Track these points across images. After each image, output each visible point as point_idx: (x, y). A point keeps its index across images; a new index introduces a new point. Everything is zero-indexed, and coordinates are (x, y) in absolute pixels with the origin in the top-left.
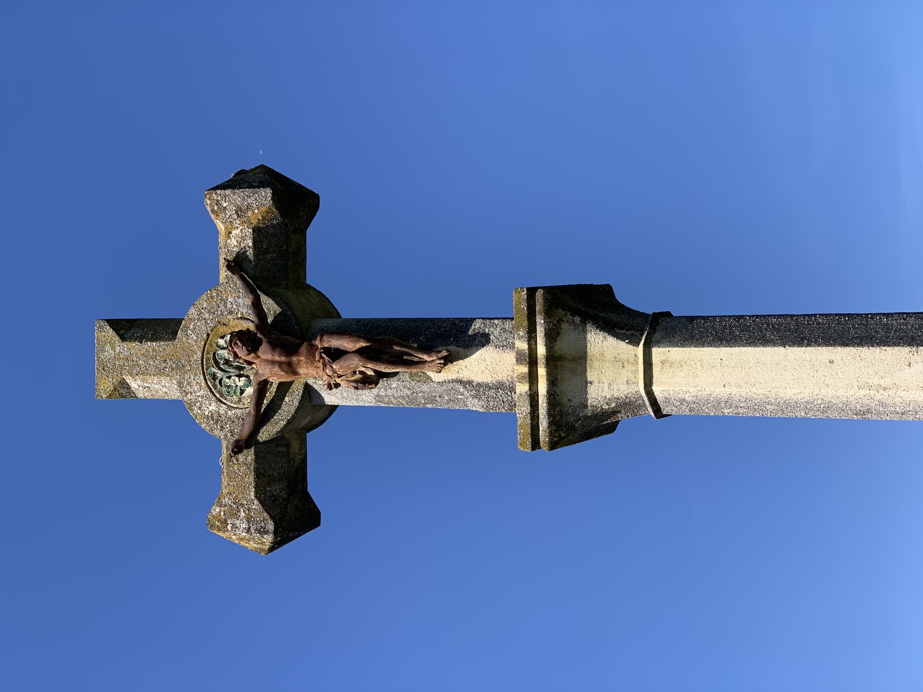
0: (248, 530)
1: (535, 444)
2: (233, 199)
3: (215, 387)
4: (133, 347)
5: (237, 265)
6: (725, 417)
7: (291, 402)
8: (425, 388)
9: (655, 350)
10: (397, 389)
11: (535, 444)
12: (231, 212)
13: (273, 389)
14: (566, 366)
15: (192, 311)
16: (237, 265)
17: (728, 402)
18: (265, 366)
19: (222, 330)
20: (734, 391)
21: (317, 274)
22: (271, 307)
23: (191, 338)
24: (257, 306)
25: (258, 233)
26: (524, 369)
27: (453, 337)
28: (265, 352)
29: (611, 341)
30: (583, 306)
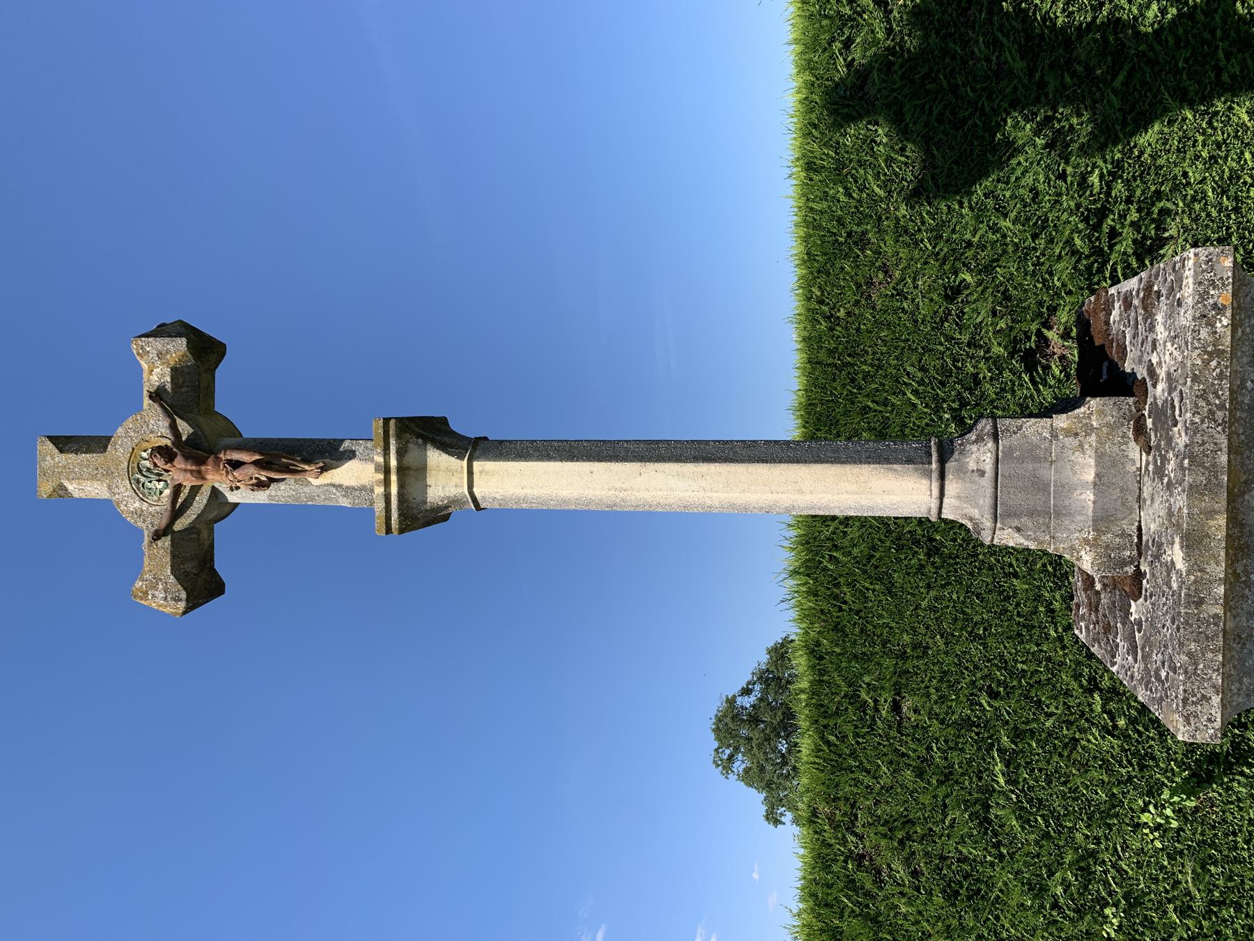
0: (165, 599)
1: (389, 530)
7: (201, 501)
8: (306, 490)
10: (285, 491)
12: (153, 354)
13: (186, 491)
14: (412, 474)
15: (120, 430)
17: (525, 500)
18: (180, 473)
19: (145, 445)
20: (529, 492)
22: (185, 428)
23: (119, 451)
24: (173, 427)
25: (175, 371)
26: (381, 476)
27: (328, 453)
28: (179, 462)
29: (445, 456)
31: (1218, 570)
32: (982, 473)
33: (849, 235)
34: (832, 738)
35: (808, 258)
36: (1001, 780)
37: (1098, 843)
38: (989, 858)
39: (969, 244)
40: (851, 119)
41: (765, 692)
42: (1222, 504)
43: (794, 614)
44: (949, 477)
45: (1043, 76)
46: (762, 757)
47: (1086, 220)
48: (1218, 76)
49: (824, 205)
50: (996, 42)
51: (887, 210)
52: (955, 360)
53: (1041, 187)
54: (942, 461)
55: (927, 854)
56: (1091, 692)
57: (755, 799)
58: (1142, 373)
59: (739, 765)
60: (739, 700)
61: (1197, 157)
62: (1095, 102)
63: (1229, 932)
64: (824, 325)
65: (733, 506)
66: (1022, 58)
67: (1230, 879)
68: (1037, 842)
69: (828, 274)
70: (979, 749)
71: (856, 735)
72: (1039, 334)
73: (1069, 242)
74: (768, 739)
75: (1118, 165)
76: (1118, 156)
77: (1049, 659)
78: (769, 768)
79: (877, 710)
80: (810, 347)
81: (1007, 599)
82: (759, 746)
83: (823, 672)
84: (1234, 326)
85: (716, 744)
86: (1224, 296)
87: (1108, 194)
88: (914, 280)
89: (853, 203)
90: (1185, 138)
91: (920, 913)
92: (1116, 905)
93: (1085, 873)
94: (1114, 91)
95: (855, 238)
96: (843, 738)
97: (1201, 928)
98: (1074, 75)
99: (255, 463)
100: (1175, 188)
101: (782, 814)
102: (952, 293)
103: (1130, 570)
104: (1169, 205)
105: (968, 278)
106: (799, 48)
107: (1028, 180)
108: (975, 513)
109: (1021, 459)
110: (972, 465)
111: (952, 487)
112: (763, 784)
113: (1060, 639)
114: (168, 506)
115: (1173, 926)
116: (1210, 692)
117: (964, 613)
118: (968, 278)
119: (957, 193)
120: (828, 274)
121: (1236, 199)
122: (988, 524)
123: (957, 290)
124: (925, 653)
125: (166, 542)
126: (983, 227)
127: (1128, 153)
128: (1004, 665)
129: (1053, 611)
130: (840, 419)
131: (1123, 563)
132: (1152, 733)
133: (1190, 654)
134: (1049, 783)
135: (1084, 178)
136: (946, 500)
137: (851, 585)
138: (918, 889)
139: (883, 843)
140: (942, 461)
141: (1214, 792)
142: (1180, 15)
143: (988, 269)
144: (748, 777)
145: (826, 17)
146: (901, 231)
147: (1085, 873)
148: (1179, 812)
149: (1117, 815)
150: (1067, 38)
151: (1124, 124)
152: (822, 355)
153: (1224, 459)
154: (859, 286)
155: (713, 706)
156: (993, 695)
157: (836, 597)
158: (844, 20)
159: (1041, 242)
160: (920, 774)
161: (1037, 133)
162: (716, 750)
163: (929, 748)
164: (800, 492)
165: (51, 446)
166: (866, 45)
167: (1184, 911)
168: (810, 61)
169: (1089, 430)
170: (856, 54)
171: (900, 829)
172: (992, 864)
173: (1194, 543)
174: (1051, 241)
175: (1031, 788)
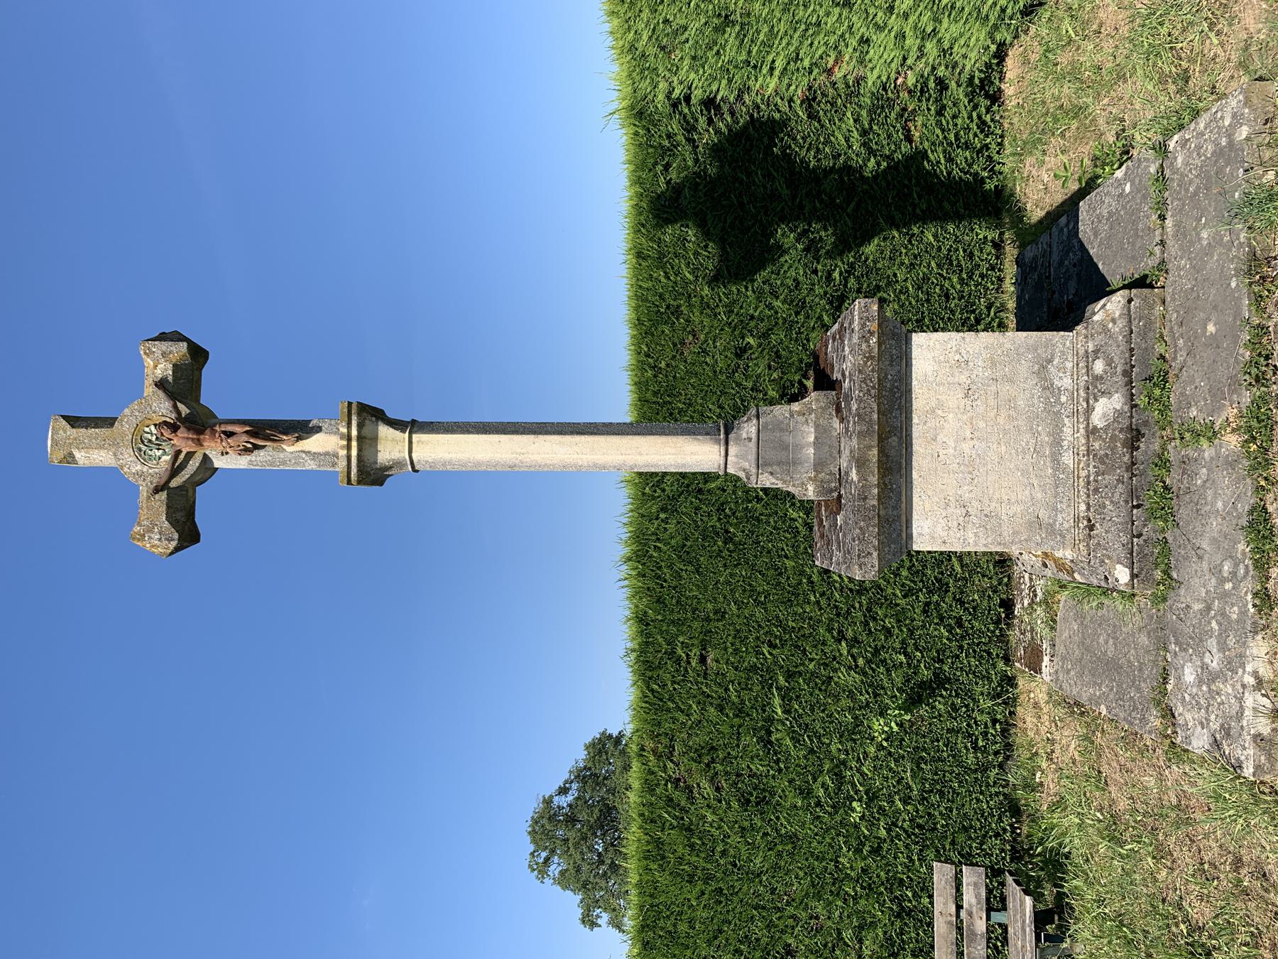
1: (349, 482)
3: (141, 455)
4: (72, 432)
5: (161, 384)
7: (194, 464)
8: (281, 455)
9: (414, 436)
10: (265, 458)
11: (349, 482)
12: (158, 354)
13: (182, 456)
14: (367, 442)
15: (127, 411)
16: (161, 384)
18: (182, 441)
19: (148, 422)
20: (453, 456)
21: (208, 397)
22: (184, 410)
23: (125, 426)
24: (175, 407)
27: (302, 429)
28: (182, 432)
29: (391, 430)
30: (371, 414)
31: (874, 479)
32: (750, 439)
33: (668, 307)
34: (655, 687)
35: (638, 323)
36: (779, 711)
37: (848, 754)
39: (752, 317)
40: (668, 221)
41: (582, 790)
42: (875, 443)
43: (627, 592)
44: (731, 443)
45: (801, 201)
46: (578, 857)
47: (831, 303)
48: (914, 210)
49: (650, 284)
50: (770, 174)
52: (743, 401)
53: (801, 279)
54: (727, 434)
55: (727, 773)
57: (571, 901)
58: (840, 377)
59: (554, 869)
60: (556, 799)
62: (836, 222)
64: (650, 373)
65: (595, 465)
67: (936, 774)
68: (805, 757)
69: (653, 335)
70: (763, 688)
71: (674, 682)
72: (800, 382)
73: (820, 318)
74: (585, 838)
75: (852, 266)
76: (851, 260)
78: (585, 868)
79: (689, 663)
80: (640, 389)
81: (780, 574)
82: (577, 845)
83: (648, 635)
84: (880, 344)
85: (532, 848)
86: (873, 326)
87: (845, 286)
89: (671, 284)
90: (894, 250)
92: (860, 800)
93: (839, 778)
94: (848, 215)
95: (672, 309)
99: (246, 432)
100: (889, 284)
101: (598, 917)
102: (741, 352)
103: (835, 494)
104: (885, 295)
106: (632, 167)
107: (792, 273)
108: (746, 465)
109: (773, 430)
110: (745, 436)
112: (579, 885)
113: (818, 602)
114: (168, 467)
115: (898, 812)
116: (872, 550)
117: (750, 585)
119: (744, 280)
120: (653, 335)
121: (928, 293)
122: (754, 471)
124: (723, 617)
126: (762, 306)
127: (857, 258)
128: (780, 624)
130: (660, 408)
131: (832, 491)
132: (882, 669)
133: (861, 528)
134: (812, 710)
135: (829, 274)
136: (729, 458)
137: (670, 567)
138: (720, 801)
139: (694, 765)
141: (923, 710)
142: (889, 167)
143: (765, 335)
144: (564, 880)
146: (705, 306)
148: (900, 725)
150: (817, 177)
151: (855, 238)
152: (649, 395)
153: (876, 416)
154: (675, 345)
155: (530, 807)
156: (772, 645)
157: (659, 577)
158: (664, 151)
160: (721, 709)
161: (798, 240)
162: (532, 854)
163: (727, 690)
165: (64, 422)
166: (681, 169)
167: (905, 801)
168: (640, 177)
169: (811, 411)
170: (673, 175)
171: (706, 754)
172: (773, 777)
173: (861, 463)
175: (800, 716)
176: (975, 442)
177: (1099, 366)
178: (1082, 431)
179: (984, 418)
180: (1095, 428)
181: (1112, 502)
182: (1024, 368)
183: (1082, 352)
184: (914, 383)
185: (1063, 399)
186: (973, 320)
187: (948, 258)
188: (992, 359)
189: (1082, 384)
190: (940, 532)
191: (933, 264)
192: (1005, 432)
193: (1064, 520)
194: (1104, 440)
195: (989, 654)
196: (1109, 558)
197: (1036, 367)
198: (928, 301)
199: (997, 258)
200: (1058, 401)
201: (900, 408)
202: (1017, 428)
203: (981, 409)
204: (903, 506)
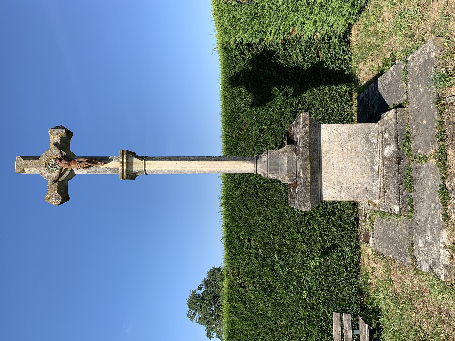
0: (55, 200)
1: (123, 178)
2: (55, 131)
3: (48, 170)
6: (158, 174)
7: (67, 173)
8: (99, 169)
10: (93, 170)
11: (123, 178)
13: (63, 170)
14: (129, 164)
15: (44, 154)
16: (56, 144)
17: (159, 171)
18: (63, 164)
19: (51, 158)
20: (160, 169)
22: (64, 153)
23: (43, 159)
24: (61, 152)
25: (61, 138)
26: (121, 164)
27: (106, 160)
28: (63, 161)
29: (138, 160)
30: (131, 154)
31: (309, 176)
32: (265, 162)
33: (235, 115)
34: (233, 250)
35: (225, 121)
36: (277, 258)
37: (301, 274)
38: (274, 281)
39: (265, 119)
40: (235, 86)
41: (206, 288)
42: (309, 163)
44: (258, 163)
47: (292, 114)
48: (321, 81)
50: (270, 69)
51: (245, 110)
52: (262, 148)
53: (282, 105)
54: (257, 160)
56: (298, 233)
57: (203, 329)
58: (296, 140)
59: (197, 317)
60: (197, 291)
61: (317, 100)
63: (333, 294)
64: (229, 139)
65: (210, 171)
66: (277, 74)
67: (333, 280)
68: (286, 275)
69: (230, 125)
70: (271, 250)
71: (239, 249)
72: (282, 141)
73: (289, 119)
74: (207, 306)
75: (299, 100)
77: (287, 225)
78: (208, 316)
79: (244, 241)
80: (226, 144)
81: (276, 209)
83: (230, 232)
84: (310, 128)
85: (188, 309)
86: (307, 122)
87: (297, 108)
88: (252, 127)
90: (314, 95)
91: (257, 298)
92: (306, 290)
93: (298, 282)
94: (298, 83)
96: (236, 250)
97: (326, 294)
98: (288, 78)
99: (86, 161)
100: (313, 107)
101: (213, 334)
102: (261, 131)
103: (295, 181)
104: (311, 111)
105: (265, 127)
106: (222, 67)
107: (279, 103)
108: (264, 171)
109: (273, 158)
110: (263, 160)
111: (259, 165)
112: (206, 323)
113: (290, 219)
115: (320, 294)
116: (308, 201)
118: (265, 127)
119: (262, 106)
120: (230, 125)
121: (326, 110)
122: (266, 173)
123: (262, 130)
124: (256, 225)
125: (56, 184)
126: (268, 115)
127: (302, 98)
128: (277, 227)
129: (288, 212)
130: (233, 151)
131: (294, 180)
132: (313, 243)
133: (304, 193)
134: (289, 258)
137: (237, 207)
138: (256, 291)
140: (257, 160)
141: (328, 257)
142: (312, 66)
143: (270, 125)
144: (200, 321)
145: (229, 60)
146: (248, 115)
147: (298, 282)
148: (320, 263)
149: (306, 266)
150: (287, 70)
151: (301, 91)
152: (229, 146)
153: (309, 153)
154: (238, 129)
155: (188, 294)
156: (274, 235)
157: (233, 211)
158: (234, 61)
159: (282, 119)
160: (256, 258)
161: (280, 92)
162: (189, 312)
163: (258, 251)
164: (226, 167)
167: (322, 290)
169: (286, 152)
170: (237, 70)
171: (251, 274)
172: (275, 282)
173: (304, 170)
174: (284, 119)
175: (284, 260)
176: (344, 162)
177: (386, 135)
178: (381, 158)
179: (346, 154)
180: (386, 157)
181: (392, 183)
182: (360, 136)
183: (380, 130)
184: (322, 142)
185: (374, 147)
186: (343, 119)
187: (333, 98)
188: (349, 133)
189: (381, 142)
190: (332, 194)
191: (328, 100)
192: (354, 159)
193: (376, 189)
194: (389, 161)
195: (351, 237)
196: (392, 202)
197: (365, 136)
198: (326, 113)
199: (350, 97)
200: (372, 147)
201: (317, 150)
202: (358, 157)
203: (346, 151)
204: (319, 184)
